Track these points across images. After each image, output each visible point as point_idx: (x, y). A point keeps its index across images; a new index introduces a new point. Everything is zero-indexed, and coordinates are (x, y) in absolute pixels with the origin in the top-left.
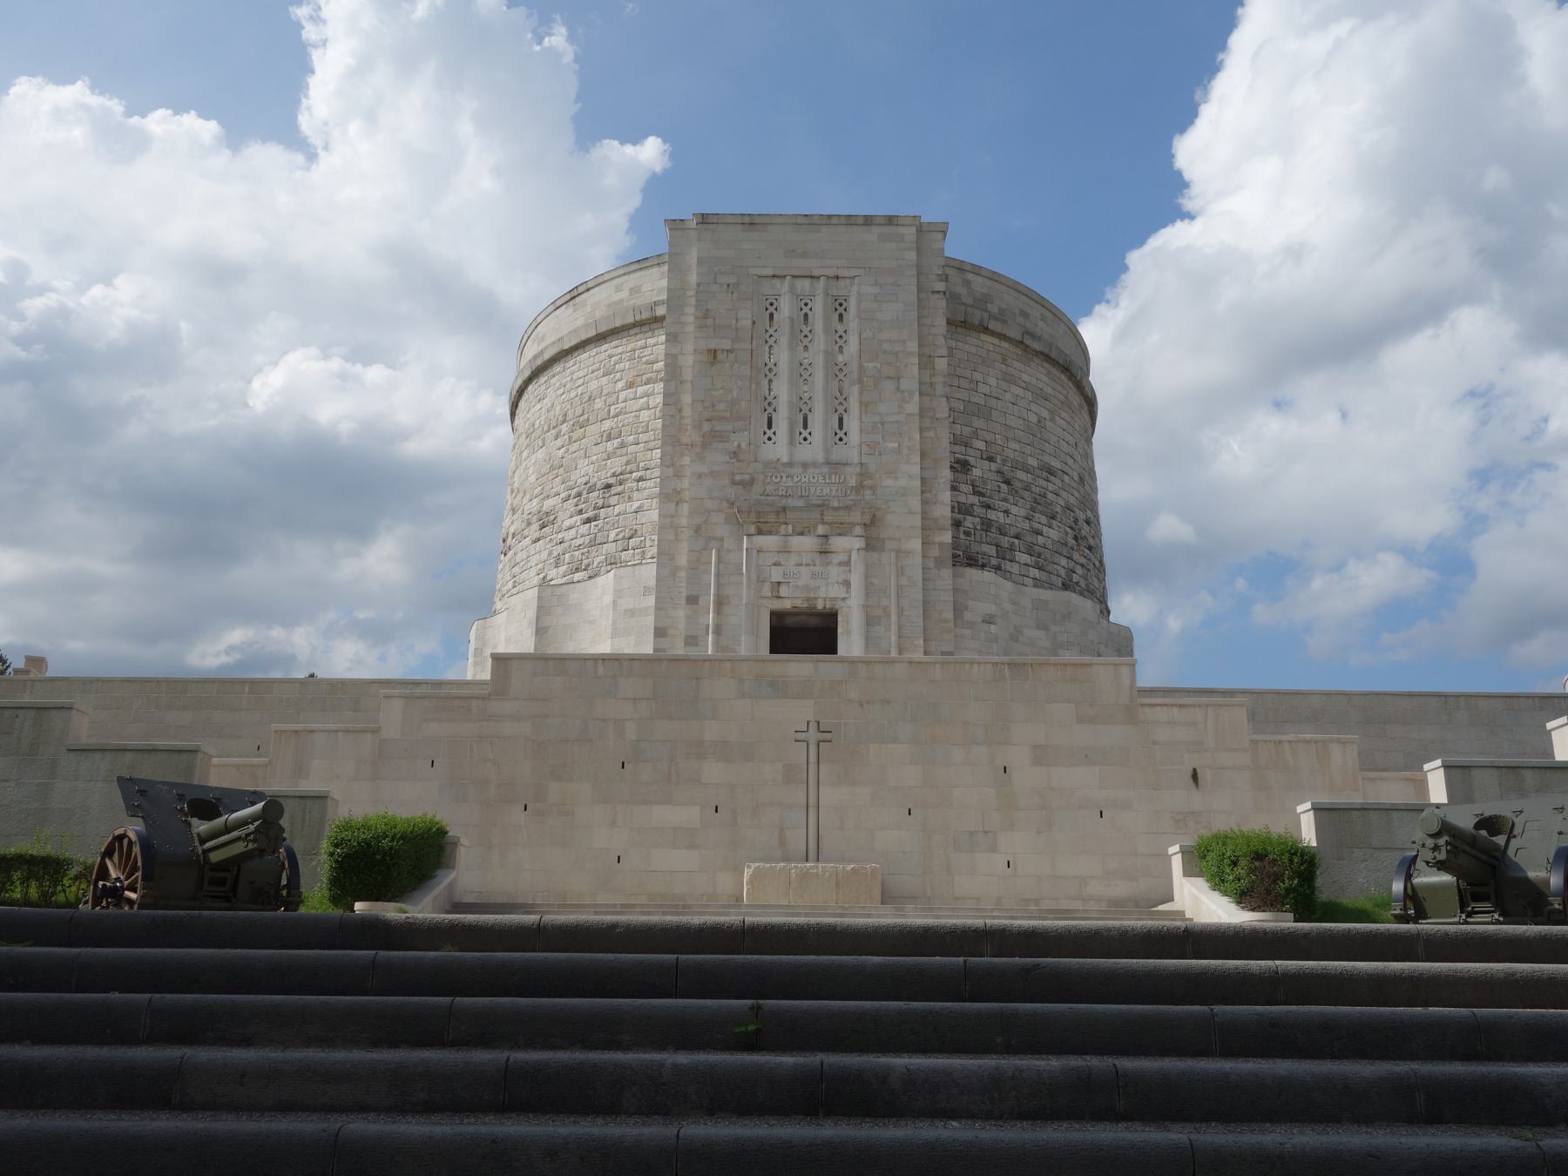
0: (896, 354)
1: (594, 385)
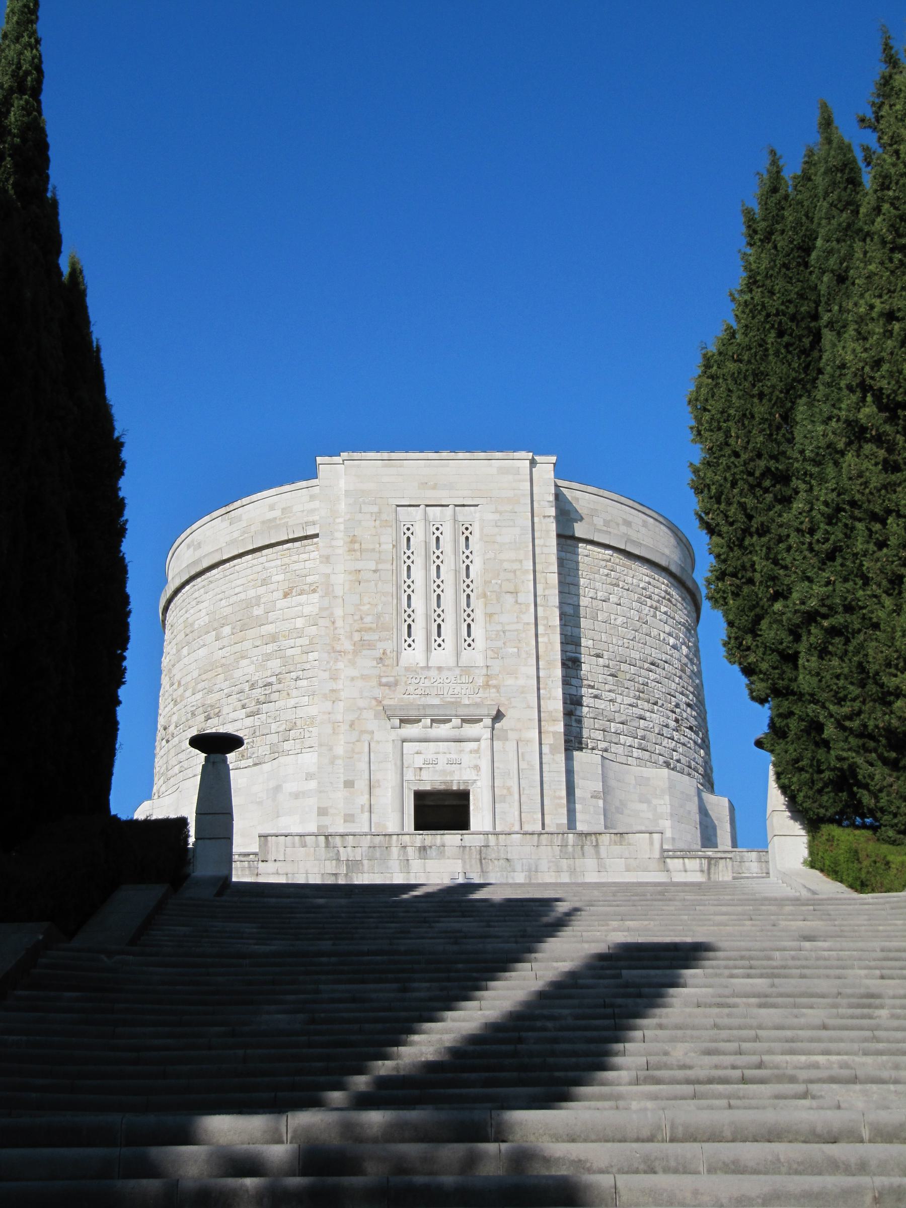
0: (515, 572)
1: (252, 593)
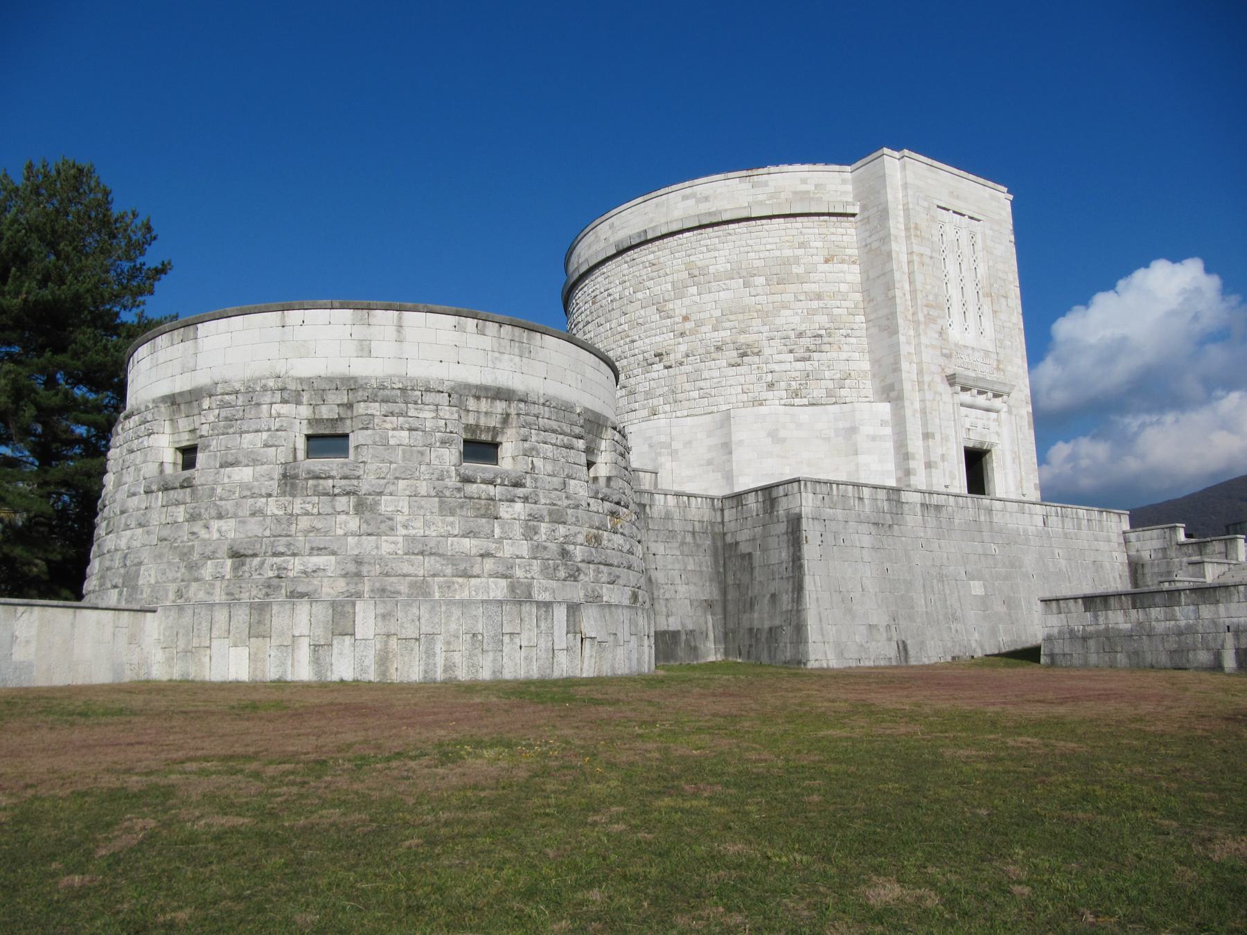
1: (788, 253)
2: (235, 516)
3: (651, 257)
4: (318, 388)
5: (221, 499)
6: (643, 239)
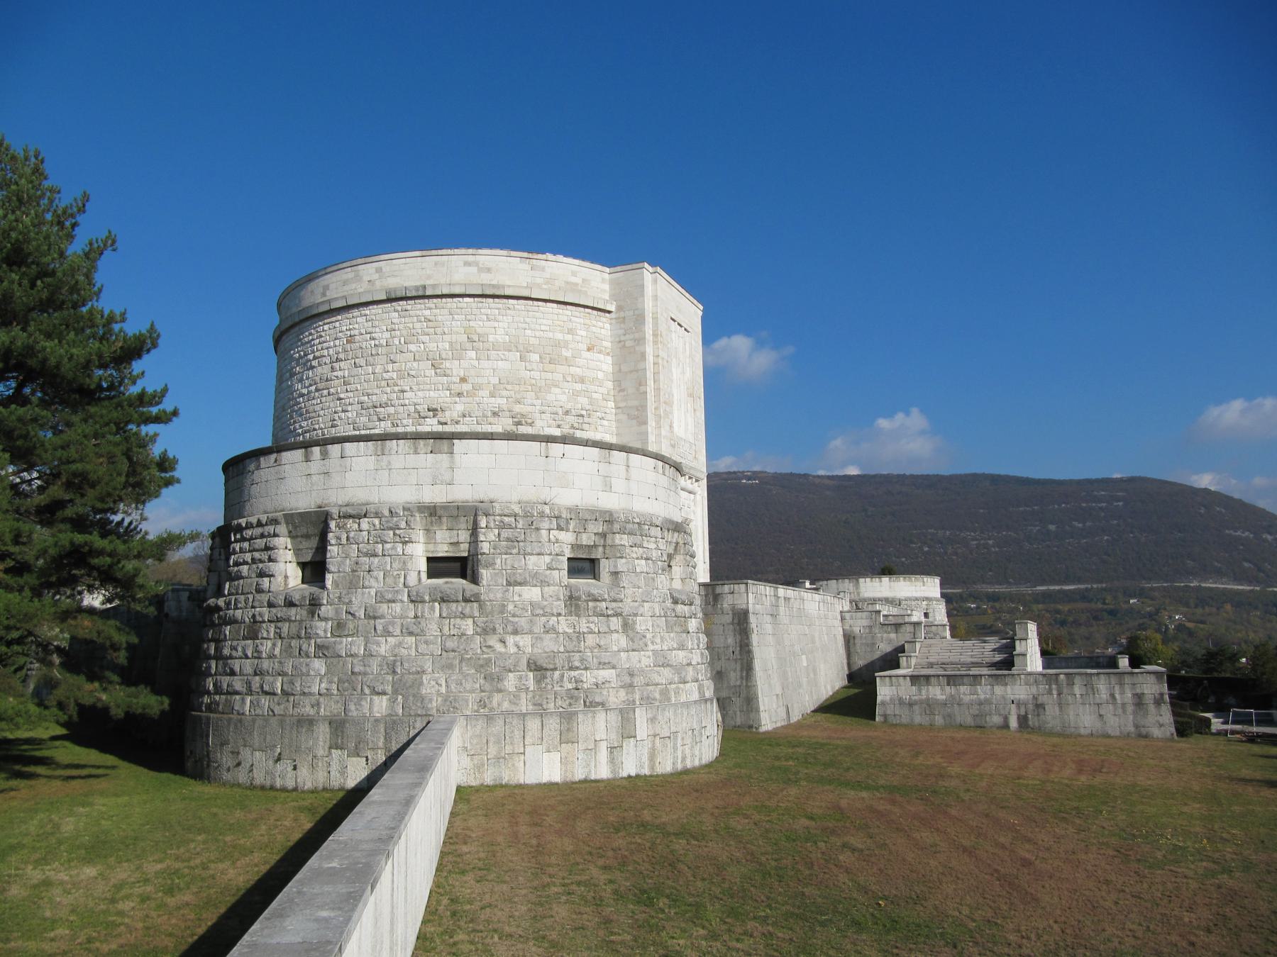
1: (559, 336)
2: (531, 632)
3: (427, 312)
4: (579, 517)
5: (514, 616)
6: (420, 293)
